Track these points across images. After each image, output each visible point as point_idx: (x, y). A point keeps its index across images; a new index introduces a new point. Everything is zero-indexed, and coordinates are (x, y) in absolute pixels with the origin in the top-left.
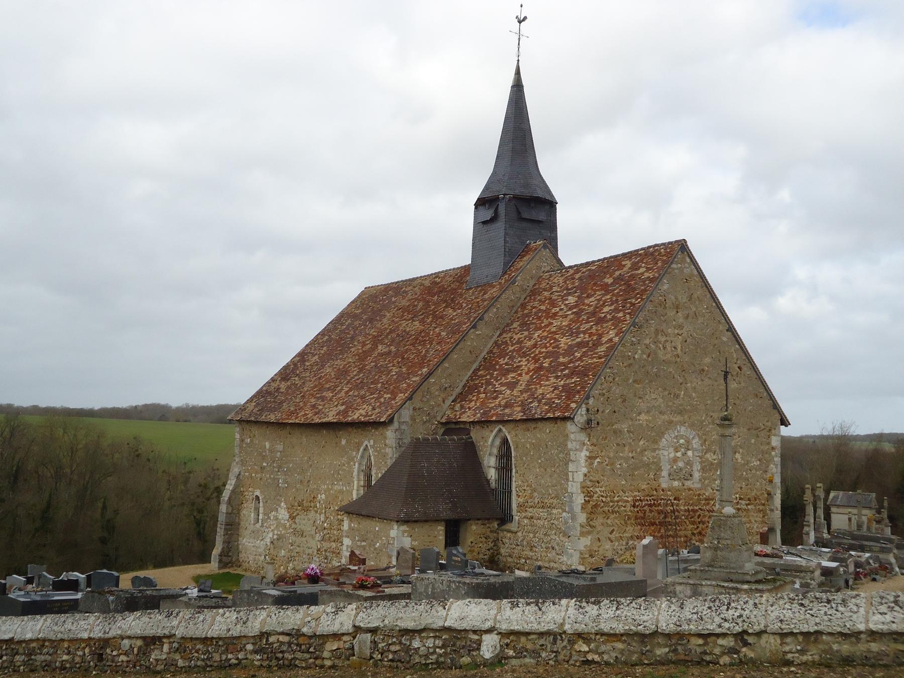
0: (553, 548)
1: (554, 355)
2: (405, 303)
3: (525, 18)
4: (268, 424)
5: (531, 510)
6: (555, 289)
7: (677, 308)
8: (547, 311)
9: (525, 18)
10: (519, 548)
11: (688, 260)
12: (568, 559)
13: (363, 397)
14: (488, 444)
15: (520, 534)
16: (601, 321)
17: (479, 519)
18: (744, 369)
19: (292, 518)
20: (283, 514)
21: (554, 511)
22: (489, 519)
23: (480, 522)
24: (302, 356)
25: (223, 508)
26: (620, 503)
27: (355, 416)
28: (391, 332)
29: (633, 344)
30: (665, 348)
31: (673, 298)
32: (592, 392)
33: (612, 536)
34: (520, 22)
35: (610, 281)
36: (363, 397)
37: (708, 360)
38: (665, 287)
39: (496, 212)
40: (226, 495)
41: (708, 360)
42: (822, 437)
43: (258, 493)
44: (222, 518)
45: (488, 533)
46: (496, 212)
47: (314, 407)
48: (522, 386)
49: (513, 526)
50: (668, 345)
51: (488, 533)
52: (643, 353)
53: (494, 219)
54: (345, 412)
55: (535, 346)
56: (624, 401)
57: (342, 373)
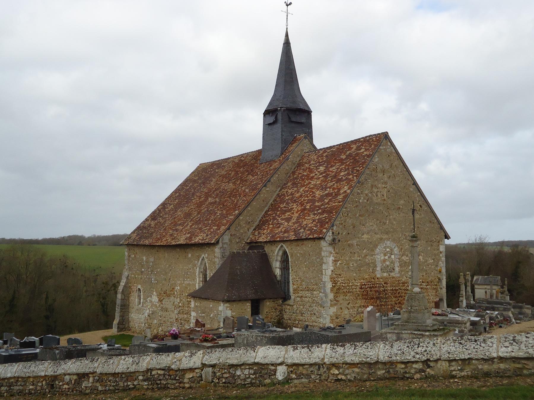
0: (315, 314)
1: (313, 201)
2: (223, 173)
3: (290, 4)
4: (144, 246)
5: (301, 292)
6: (312, 162)
7: (383, 172)
8: (308, 176)
9: (290, 4)
10: (295, 314)
11: (389, 144)
12: (324, 320)
13: (200, 229)
14: (275, 255)
15: (295, 306)
16: (340, 180)
17: (271, 299)
18: (423, 206)
19: (160, 301)
20: (155, 299)
21: (315, 293)
22: (276, 298)
23: (272, 300)
24: (164, 205)
25: (119, 296)
26: (353, 287)
27: (197, 240)
28: (216, 190)
29: (358, 194)
30: (377, 196)
31: (381, 166)
32: (335, 223)
33: (349, 306)
34: (287, 5)
35: (344, 157)
36: (200, 229)
37: (402, 202)
38: (377, 160)
39: (276, 118)
40: (120, 288)
41: (402, 202)
42: (468, 244)
43: (139, 287)
44: (118, 302)
45: (277, 307)
46: (276, 118)
47: (171, 235)
48: (294, 220)
49: (291, 302)
50: (379, 194)
51: (277, 307)
52: (364, 199)
53: (275, 123)
54: (190, 238)
55: (301, 196)
56: (354, 227)
57: (188, 215)
